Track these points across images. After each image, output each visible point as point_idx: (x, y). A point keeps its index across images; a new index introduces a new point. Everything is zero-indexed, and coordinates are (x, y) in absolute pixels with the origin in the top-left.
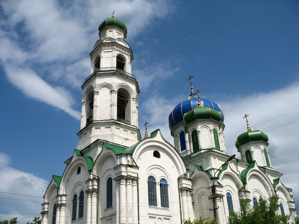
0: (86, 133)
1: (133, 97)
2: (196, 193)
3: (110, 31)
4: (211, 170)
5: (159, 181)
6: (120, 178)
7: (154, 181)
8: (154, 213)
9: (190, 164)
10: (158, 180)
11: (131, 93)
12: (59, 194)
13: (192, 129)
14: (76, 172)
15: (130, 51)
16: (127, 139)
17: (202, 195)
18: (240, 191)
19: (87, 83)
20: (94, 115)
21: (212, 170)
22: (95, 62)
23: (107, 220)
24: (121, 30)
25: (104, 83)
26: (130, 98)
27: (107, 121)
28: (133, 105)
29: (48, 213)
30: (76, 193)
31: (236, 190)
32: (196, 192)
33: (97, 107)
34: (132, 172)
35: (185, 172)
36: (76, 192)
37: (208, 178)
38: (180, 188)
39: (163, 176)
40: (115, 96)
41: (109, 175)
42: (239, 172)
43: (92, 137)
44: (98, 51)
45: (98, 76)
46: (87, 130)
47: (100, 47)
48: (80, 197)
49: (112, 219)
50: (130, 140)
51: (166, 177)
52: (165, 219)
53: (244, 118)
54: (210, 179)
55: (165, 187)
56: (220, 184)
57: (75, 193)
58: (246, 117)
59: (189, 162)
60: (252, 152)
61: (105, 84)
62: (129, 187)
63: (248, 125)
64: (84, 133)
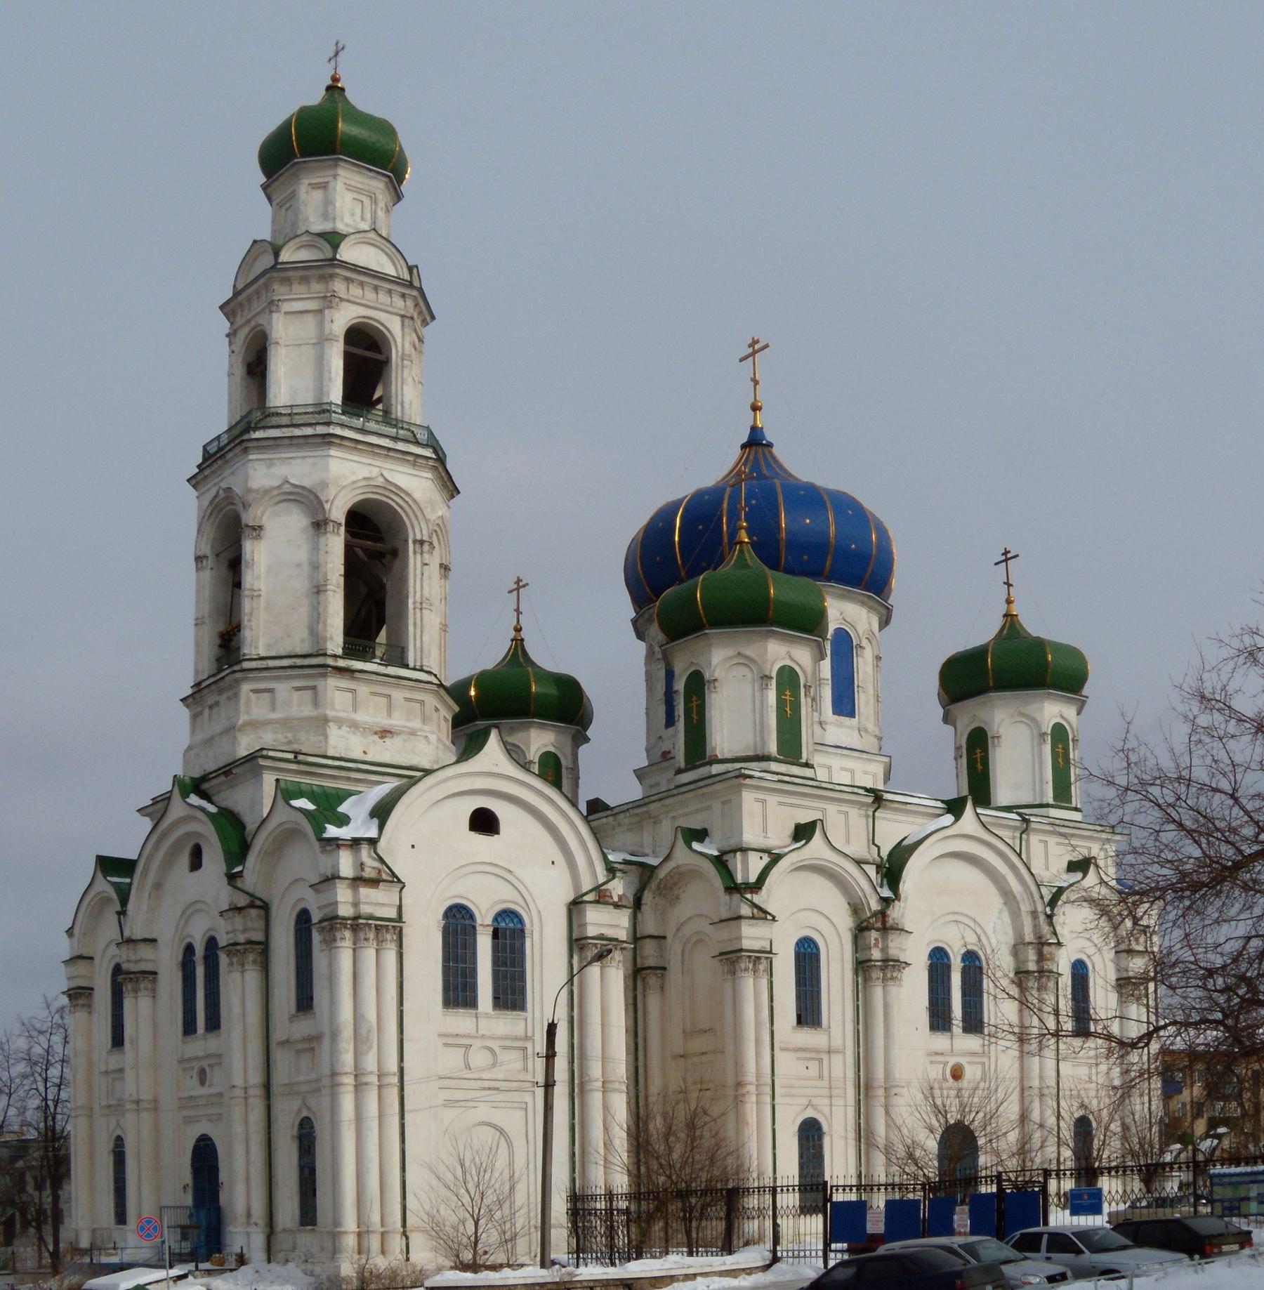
0: (217, 704)
1: (419, 537)
2: (675, 935)
3: (314, 186)
4: (732, 855)
5: (489, 921)
6: (332, 922)
7: (467, 922)
8: (460, 1031)
9: (667, 812)
10: (484, 918)
11: (407, 515)
12: (126, 934)
13: (688, 668)
14: (185, 860)
15: (415, 293)
16: (384, 733)
17: (696, 943)
18: (860, 930)
19: (213, 472)
20: (247, 634)
21: (738, 854)
22: (247, 349)
23: (298, 1052)
24: (370, 170)
25: (287, 486)
26: (407, 541)
27: (299, 662)
28: (419, 572)
29: (90, 994)
30: (188, 940)
31: (845, 922)
32: (678, 930)
33: (256, 595)
34: (378, 902)
35: (601, 879)
36: (189, 936)
37: (718, 883)
38: (574, 937)
39: (508, 898)
40: (335, 545)
41: (298, 901)
42: (879, 848)
43: (239, 730)
44: (257, 306)
45: (258, 448)
46: (220, 692)
47: (267, 286)
48: (206, 958)
49: (313, 1049)
50: (399, 734)
51: (524, 905)
52: (504, 1048)
53: (996, 564)
54: (722, 889)
55: (513, 938)
56: (766, 912)
57: (184, 939)
58: (1006, 560)
59: (663, 806)
60: (993, 738)
61: (287, 488)
62: (369, 954)
63: (1009, 602)
64: (209, 703)
